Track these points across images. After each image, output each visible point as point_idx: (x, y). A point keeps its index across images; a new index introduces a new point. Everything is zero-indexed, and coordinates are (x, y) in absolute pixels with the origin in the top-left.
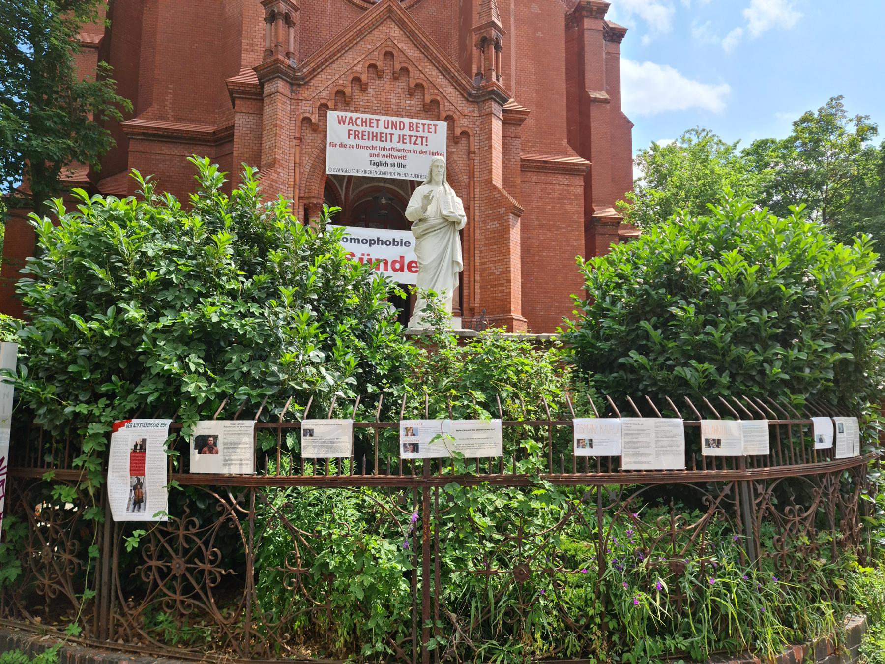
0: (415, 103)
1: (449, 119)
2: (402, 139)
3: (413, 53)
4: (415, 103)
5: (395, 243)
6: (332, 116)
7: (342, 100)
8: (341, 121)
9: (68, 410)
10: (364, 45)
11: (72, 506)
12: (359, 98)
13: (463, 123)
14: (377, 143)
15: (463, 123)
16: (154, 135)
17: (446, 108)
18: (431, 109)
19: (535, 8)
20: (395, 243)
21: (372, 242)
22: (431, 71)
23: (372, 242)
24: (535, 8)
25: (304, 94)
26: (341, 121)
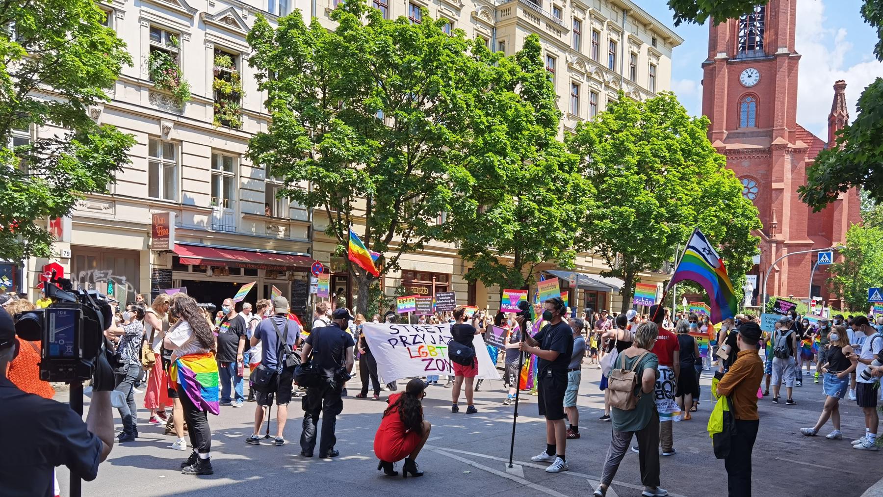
13: (765, 248)
15: (765, 248)
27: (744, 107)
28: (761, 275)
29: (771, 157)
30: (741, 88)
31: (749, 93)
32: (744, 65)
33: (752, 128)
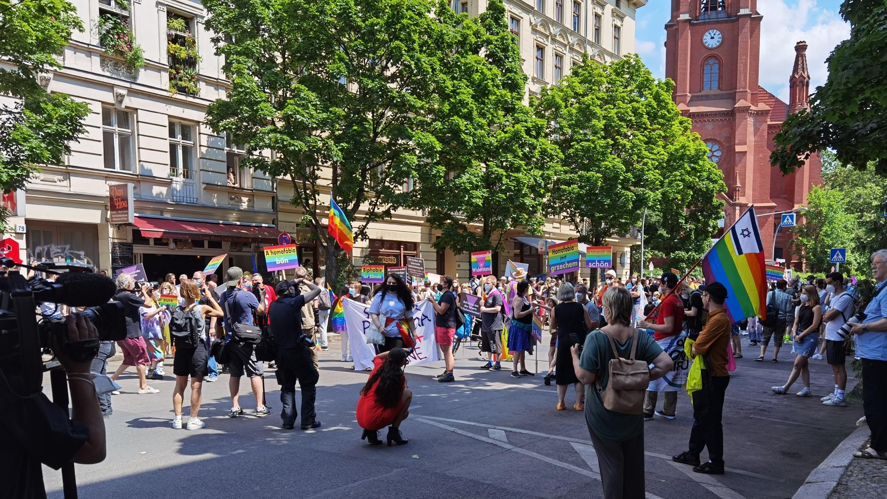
13: (729, 211)
15: (729, 211)
19: (761, 155)
24: (761, 155)
27: (707, 68)
29: (734, 120)
30: (704, 50)
31: (712, 55)
32: (707, 26)
33: (715, 91)
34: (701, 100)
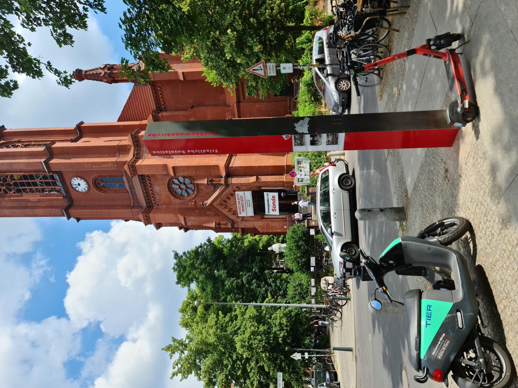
0: (232, 198)
1: (234, 191)
2: (242, 201)
3: (219, 200)
4: (232, 198)
5: (268, 201)
6: (239, 215)
7: (235, 213)
8: (240, 213)
9: (477, 370)
10: (220, 209)
11: (196, 302)
12: (234, 209)
14: (244, 206)
15: (234, 188)
16: (100, 207)
17: (231, 191)
18: (233, 195)
20: (268, 201)
21: (269, 206)
22: (223, 195)
23: (269, 206)
25: (236, 220)
26: (240, 213)
28: (263, 188)
30: (91, 191)
34: (135, 192)
